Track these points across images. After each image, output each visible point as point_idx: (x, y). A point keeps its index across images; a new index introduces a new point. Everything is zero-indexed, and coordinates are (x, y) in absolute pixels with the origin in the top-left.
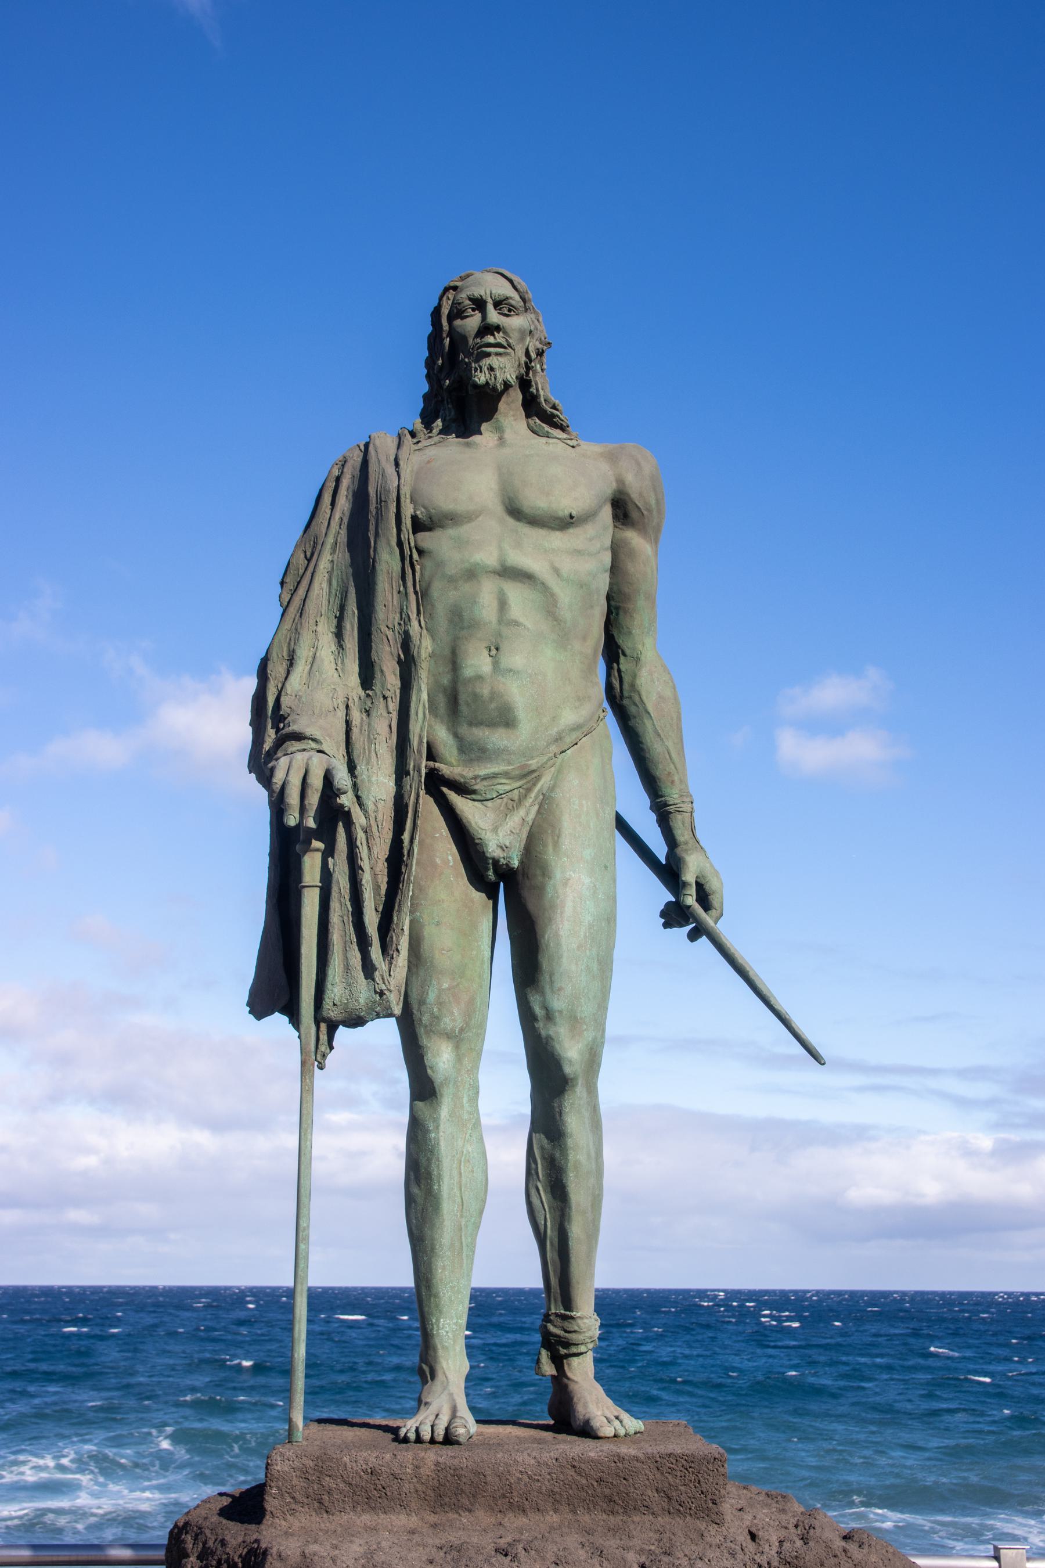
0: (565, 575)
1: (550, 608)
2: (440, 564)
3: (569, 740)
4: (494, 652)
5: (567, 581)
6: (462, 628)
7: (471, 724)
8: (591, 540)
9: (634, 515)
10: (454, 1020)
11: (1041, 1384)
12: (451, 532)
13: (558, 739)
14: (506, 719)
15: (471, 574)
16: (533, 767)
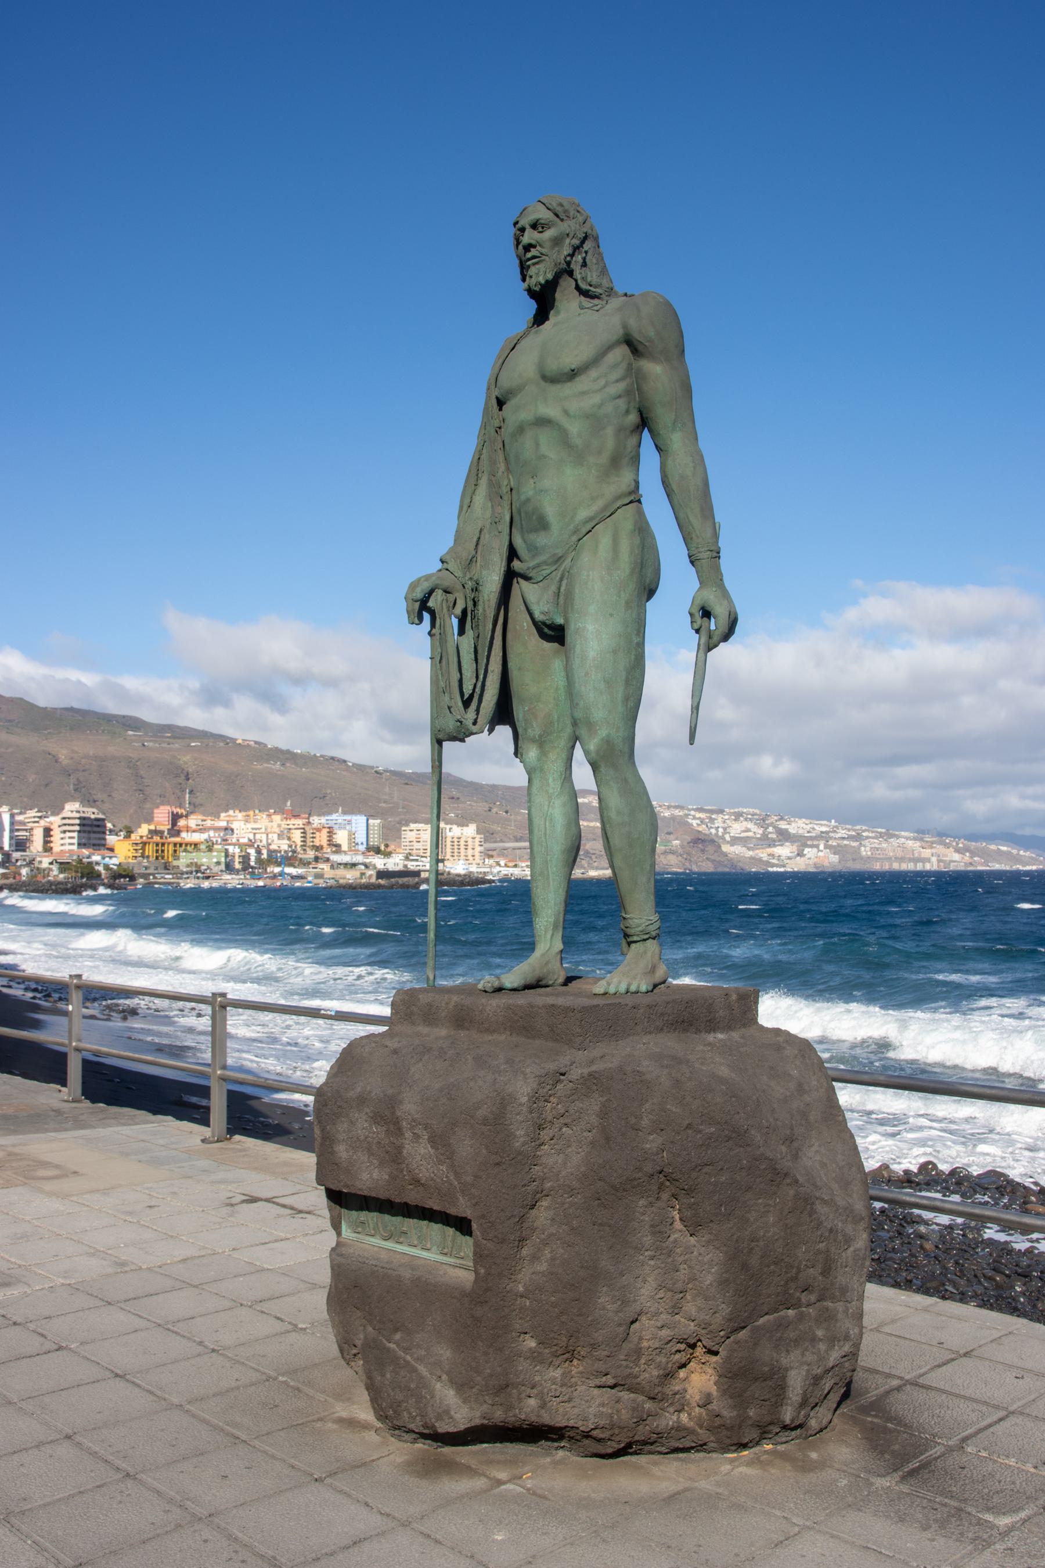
1: (564, 440)
3: (584, 530)
9: (640, 348)
11: (1028, 1094)
14: (543, 525)
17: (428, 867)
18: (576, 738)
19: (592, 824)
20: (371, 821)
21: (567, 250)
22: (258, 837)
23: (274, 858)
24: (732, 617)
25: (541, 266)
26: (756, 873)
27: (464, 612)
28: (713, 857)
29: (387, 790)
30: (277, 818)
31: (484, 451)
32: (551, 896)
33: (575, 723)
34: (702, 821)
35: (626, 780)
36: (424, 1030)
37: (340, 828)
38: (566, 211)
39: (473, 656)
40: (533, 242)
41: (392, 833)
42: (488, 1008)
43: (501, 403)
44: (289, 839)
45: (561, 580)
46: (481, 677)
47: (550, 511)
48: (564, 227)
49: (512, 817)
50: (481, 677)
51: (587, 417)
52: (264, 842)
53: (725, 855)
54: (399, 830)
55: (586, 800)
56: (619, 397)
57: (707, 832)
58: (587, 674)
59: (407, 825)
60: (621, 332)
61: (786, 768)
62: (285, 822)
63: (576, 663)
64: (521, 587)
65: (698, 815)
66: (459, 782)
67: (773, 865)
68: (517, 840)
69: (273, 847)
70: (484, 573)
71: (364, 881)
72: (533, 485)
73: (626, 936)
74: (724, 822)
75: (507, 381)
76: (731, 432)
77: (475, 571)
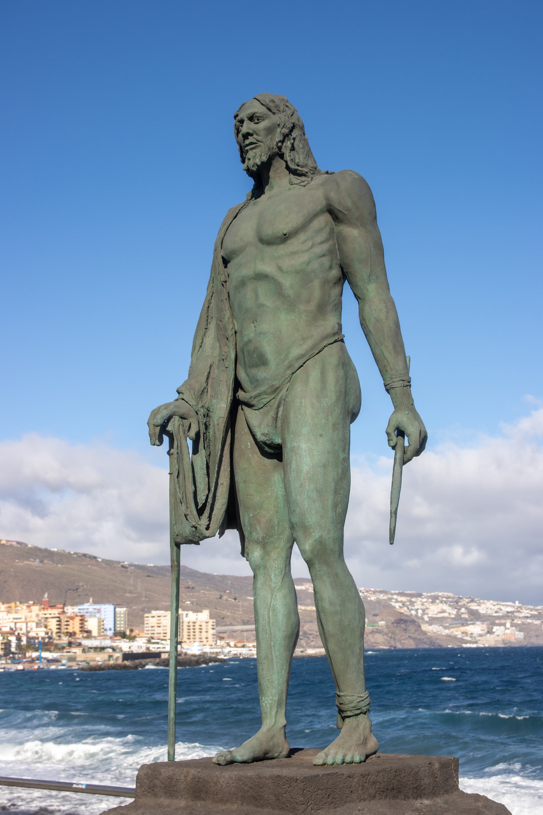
0: (285, 270)
1: (279, 291)
3: (297, 365)
5: (287, 273)
8: (303, 243)
9: (340, 216)
10: (258, 534)
13: (290, 366)
14: (262, 362)
16: (277, 386)
17: (168, 648)
18: (293, 540)
19: (309, 608)
20: (118, 610)
21: (278, 137)
22: (18, 625)
23: (32, 644)
24: (423, 435)
25: (257, 151)
26: (453, 649)
27: (198, 434)
28: (414, 636)
29: (132, 581)
30: (36, 609)
31: (213, 301)
32: (275, 677)
33: (292, 527)
34: (404, 604)
35: (337, 575)
36: (165, 801)
37: (91, 616)
38: (277, 106)
39: (205, 471)
40: (251, 131)
41: (136, 619)
42: (221, 780)
43: (226, 262)
44: (46, 627)
45: (278, 407)
46: (213, 489)
47: (268, 349)
48: (275, 119)
49: (240, 603)
50: (213, 489)
51: (298, 272)
52: (24, 631)
53: (425, 633)
54: (142, 617)
55: (303, 588)
56: (324, 255)
57: (408, 613)
58: (301, 485)
59: (149, 612)
60: (324, 203)
61: (475, 556)
62: (43, 612)
63: (292, 476)
64: (245, 413)
65: (400, 599)
66: (194, 574)
67: (467, 642)
68: (245, 623)
69: (32, 634)
70: (214, 401)
71: (112, 662)
72: (254, 328)
73: (341, 711)
74: (423, 605)
75: (230, 244)
76: (417, 285)
77: (207, 399)
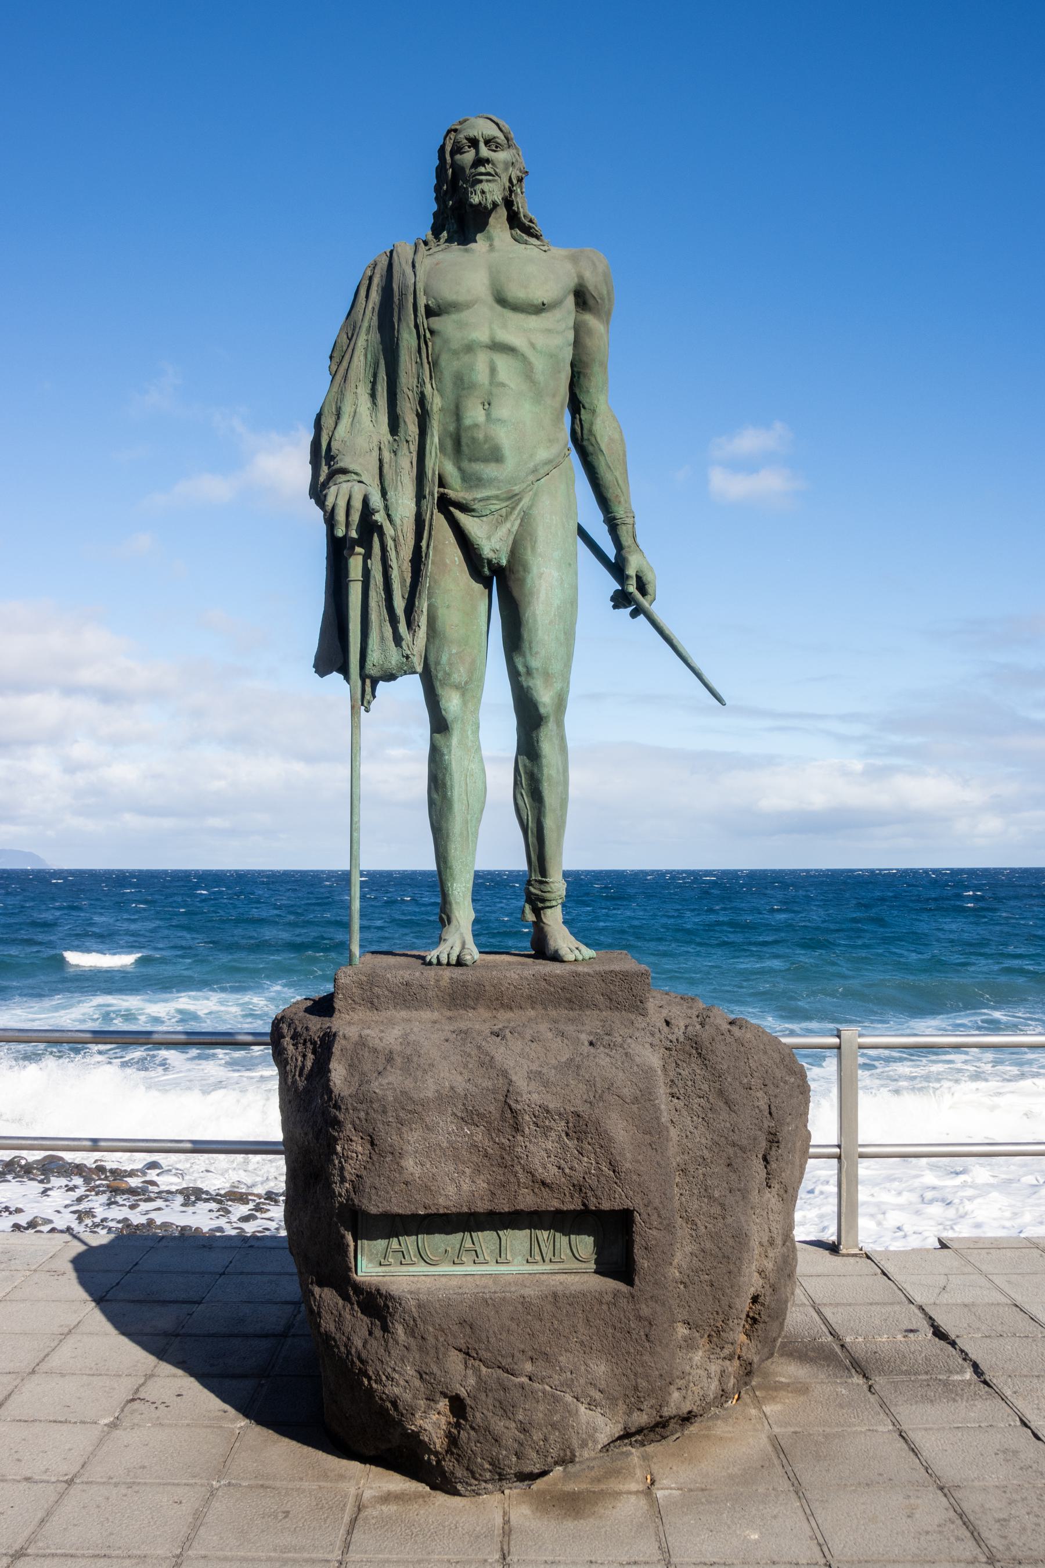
1: (528, 372)
2: (446, 341)
4: (487, 406)
5: (541, 353)
6: (463, 389)
7: (470, 460)
8: (558, 321)
9: (591, 302)
12: (454, 317)
13: (535, 471)
14: (495, 456)
15: (469, 348)
16: (517, 492)
